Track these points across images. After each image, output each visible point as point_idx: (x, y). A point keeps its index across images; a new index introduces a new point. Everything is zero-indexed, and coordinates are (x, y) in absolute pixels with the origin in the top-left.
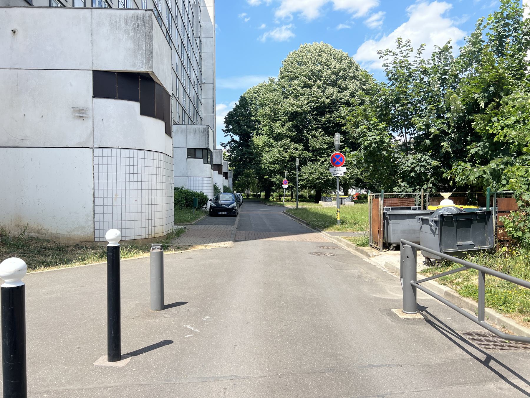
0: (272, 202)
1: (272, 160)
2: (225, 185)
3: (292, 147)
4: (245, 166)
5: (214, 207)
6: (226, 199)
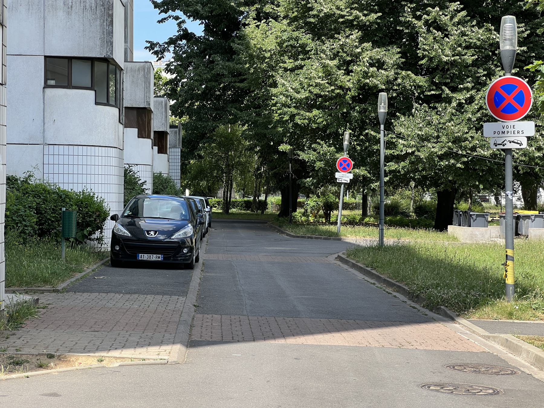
0: (302, 224)
1: (303, 95)
2: (157, 171)
3: (366, 57)
4: (220, 113)
5: (126, 239)
6: (162, 213)
